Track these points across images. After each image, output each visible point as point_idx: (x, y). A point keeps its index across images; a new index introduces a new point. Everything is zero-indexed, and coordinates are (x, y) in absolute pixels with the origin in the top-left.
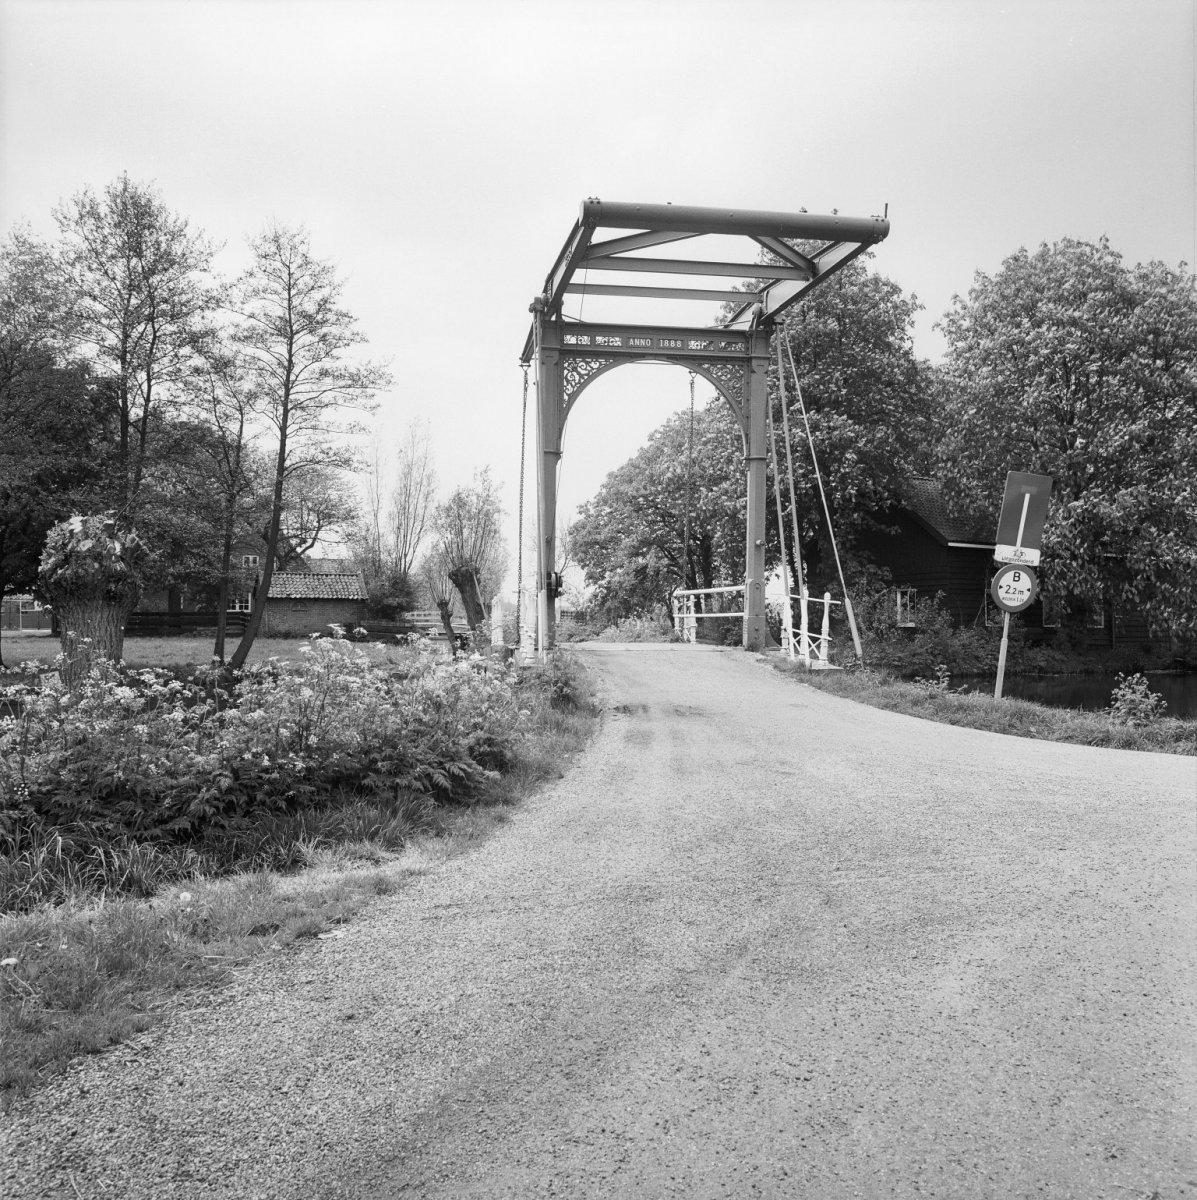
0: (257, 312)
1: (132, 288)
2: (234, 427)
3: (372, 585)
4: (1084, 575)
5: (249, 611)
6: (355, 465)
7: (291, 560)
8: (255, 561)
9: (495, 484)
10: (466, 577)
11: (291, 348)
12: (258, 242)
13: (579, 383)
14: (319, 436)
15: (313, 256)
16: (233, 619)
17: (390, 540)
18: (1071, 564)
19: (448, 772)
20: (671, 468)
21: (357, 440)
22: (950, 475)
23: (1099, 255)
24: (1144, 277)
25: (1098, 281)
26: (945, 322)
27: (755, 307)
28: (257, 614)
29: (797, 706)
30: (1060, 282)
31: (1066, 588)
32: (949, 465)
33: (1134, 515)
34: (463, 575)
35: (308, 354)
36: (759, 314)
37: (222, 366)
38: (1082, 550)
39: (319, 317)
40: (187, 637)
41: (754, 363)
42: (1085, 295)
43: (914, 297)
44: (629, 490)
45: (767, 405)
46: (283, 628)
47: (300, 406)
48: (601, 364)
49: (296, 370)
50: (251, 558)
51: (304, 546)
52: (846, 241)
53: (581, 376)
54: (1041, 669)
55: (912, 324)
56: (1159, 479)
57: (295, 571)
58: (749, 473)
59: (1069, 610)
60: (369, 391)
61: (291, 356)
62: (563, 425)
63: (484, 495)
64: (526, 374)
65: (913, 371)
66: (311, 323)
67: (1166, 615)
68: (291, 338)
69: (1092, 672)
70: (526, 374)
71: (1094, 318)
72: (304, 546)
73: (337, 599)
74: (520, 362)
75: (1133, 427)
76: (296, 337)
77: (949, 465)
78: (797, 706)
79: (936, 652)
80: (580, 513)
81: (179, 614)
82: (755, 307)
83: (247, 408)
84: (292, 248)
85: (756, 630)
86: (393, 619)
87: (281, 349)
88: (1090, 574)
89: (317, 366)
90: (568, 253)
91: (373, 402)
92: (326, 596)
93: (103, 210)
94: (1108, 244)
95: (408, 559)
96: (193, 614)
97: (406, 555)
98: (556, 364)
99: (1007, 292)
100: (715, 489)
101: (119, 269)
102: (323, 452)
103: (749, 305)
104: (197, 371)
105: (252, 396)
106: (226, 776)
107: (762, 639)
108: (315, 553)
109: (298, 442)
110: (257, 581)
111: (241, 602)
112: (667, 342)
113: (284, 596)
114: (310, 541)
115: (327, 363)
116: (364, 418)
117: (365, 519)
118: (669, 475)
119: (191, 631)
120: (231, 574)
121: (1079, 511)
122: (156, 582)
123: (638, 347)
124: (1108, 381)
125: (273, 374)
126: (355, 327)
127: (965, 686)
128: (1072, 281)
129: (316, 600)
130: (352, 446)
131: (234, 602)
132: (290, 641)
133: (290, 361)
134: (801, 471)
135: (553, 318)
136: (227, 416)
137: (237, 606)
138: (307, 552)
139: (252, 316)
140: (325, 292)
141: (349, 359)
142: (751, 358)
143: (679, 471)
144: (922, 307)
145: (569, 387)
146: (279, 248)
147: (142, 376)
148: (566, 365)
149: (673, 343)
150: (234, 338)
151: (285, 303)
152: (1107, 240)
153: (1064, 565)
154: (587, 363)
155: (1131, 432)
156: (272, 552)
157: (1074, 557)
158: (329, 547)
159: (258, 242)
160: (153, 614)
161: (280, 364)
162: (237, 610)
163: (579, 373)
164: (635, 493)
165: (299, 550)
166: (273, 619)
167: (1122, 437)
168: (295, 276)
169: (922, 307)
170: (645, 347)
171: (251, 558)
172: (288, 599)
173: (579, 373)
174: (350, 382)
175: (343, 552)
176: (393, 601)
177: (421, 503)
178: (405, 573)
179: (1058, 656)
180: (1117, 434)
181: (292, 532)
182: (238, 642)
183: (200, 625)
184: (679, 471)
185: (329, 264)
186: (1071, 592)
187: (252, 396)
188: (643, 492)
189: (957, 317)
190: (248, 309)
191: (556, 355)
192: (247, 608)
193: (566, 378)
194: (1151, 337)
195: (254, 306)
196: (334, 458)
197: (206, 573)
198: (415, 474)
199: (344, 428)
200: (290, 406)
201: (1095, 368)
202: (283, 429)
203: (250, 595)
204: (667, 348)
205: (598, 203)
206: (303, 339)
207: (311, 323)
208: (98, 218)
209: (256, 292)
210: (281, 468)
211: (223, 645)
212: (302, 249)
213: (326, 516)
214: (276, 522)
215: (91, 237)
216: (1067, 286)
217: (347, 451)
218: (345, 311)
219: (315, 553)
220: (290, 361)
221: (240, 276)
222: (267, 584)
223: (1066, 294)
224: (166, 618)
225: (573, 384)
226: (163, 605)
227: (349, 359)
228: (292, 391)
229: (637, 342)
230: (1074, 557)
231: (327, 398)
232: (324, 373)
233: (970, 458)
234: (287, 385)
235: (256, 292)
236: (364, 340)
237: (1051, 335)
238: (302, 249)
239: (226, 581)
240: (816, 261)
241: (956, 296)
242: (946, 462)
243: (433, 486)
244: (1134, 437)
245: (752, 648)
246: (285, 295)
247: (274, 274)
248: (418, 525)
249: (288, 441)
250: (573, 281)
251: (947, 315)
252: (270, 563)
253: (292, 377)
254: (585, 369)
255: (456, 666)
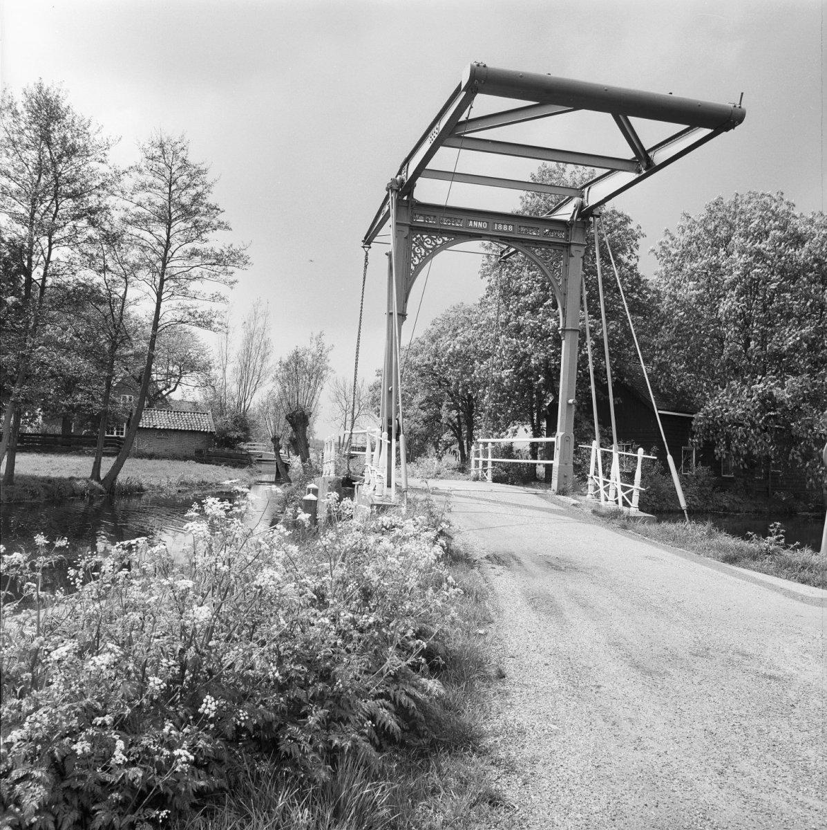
0: (143, 202)
1: (40, 169)
2: (120, 291)
3: (219, 421)
4: (760, 440)
5: (124, 436)
6: (216, 326)
7: (157, 400)
8: (130, 400)
9: (327, 346)
10: (299, 420)
11: (169, 231)
12: (147, 146)
13: (425, 255)
14: (188, 302)
15: (192, 159)
16: (110, 441)
17: (233, 388)
18: (750, 431)
19: (394, 702)
20: (451, 345)
21: (218, 306)
22: (663, 360)
23: (776, 204)
24: (811, 221)
25: (777, 223)
26: (658, 249)
27: (576, 201)
28: (129, 440)
29: (651, 558)
30: (748, 222)
31: (747, 448)
32: (663, 352)
33: (800, 397)
34: (297, 417)
35: (182, 238)
36: (581, 207)
37: (112, 239)
38: (760, 422)
39: (193, 208)
40: (75, 454)
41: (573, 248)
42: (767, 233)
43: (639, 227)
44: (417, 360)
45: (582, 285)
46: (149, 451)
47: (173, 277)
48: (443, 240)
49: (172, 249)
50: (128, 397)
51: (168, 390)
52: (700, 127)
53: (427, 250)
54: (725, 509)
55: (637, 247)
56: (818, 371)
57: (160, 408)
58: (563, 342)
59: (746, 466)
60: (230, 269)
61: (169, 238)
62: (410, 288)
63: (318, 354)
64: (367, 254)
65: (637, 282)
66: (187, 213)
67: (821, 472)
68: (170, 225)
69: (761, 512)
70: (367, 254)
71: (774, 250)
72: (168, 390)
73: (192, 431)
74: (362, 244)
75: (803, 331)
76: (173, 224)
77: (663, 352)
78: (651, 558)
79: (651, 493)
80: (378, 375)
81: (70, 436)
82: (576, 201)
83: (131, 278)
84: (175, 153)
85: (565, 476)
86: (233, 448)
87: (162, 232)
88: (765, 440)
89: (188, 247)
90: (435, 129)
91: (231, 279)
92: (183, 429)
93: (20, 108)
94: (783, 197)
95: (247, 402)
96: (81, 437)
97: (245, 400)
98: (406, 238)
99: (709, 227)
100: (485, 363)
101: (32, 155)
102: (190, 314)
103: (571, 198)
104: (90, 240)
105: (136, 267)
106: (39, 781)
107: (570, 486)
108: (176, 396)
109: (170, 306)
110: (131, 414)
111: (117, 429)
112: (500, 226)
113: (151, 427)
114: (173, 386)
115: (197, 245)
116: (224, 290)
117: (216, 372)
118: (450, 350)
119: (78, 450)
120: (109, 408)
121: (760, 391)
122: (54, 410)
123: (475, 228)
124: (784, 297)
125: (154, 251)
126: (221, 217)
127: (797, 543)
128: (756, 222)
129: (175, 431)
130: (214, 310)
131: (112, 429)
132: (153, 461)
133: (168, 241)
134: (552, 351)
135: (405, 198)
136: (114, 281)
137: (115, 433)
138: (170, 395)
139: (139, 205)
140: (200, 189)
141: (215, 241)
142: (570, 244)
143: (458, 347)
144: (644, 236)
145: (416, 259)
146: (163, 153)
147: (45, 241)
148: (414, 239)
149: (505, 228)
150: (124, 220)
151: (166, 197)
152: (782, 194)
153: (745, 431)
154: (432, 239)
155: (802, 334)
156: (144, 394)
157: (753, 426)
158: (187, 391)
159: (147, 146)
160: (51, 435)
161: (160, 244)
162: (115, 435)
163: (425, 248)
164: (420, 363)
165: (164, 393)
166: (141, 444)
167: (794, 338)
168: (175, 176)
169: (644, 236)
170: (483, 229)
171: (128, 397)
172: (154, 429)
173: (425, 248)
174: (215, 261)
175: (197, 395)
176: (235, 435)
177: (259, 363)
178: (244, 413)
179: (738, 499)
180: (790, 336)
181: (160, 378)
182: (113, 460)
183: (85, 445)
184: (458, 347)
185: (203, 167)
186: (750, 453)
187: (136, 267)
188: (426, 362)
189: (667, 246)
190: (136, 199)
191: (407, 230)
192: (122, 434)
193: (414, 251)
194: (815, 265)
195: (142, 196)
196: (199, 319)
197: (91, 406)
198: (255, 340)
199: (207, 297)
200: (165, 277)
201: (774, 287)
202: (159, 295)
203: (125, 424)
204: (505, 232)
205: (485, 66)
206: (178, 225)
207: (187, 213)
208: (15, 113)
209: (143, 186)
210: (155, 325)
211: (100, 463)
212: (182, 154)
213: (189, 365)
214: (148, 371)
215: (9, 129)
216: (752, 225)
217: (210, 314)
218: (213, 204)
219: (176, 396)
220: (168, 241)
221: (131, 165)
222: (139, 417)
223: (752, 231)
224: (59, 439)
225: (419, 255)
226: (58, 430)
227: (215, 241)
228: (168, 265)
229: (476, 224)
230: (753, 426)
231: (195, 272)
232: (195, 253)
233: (678, 348)
234: (165, 260)
235: (143, 186)
236: (227, 228)
237: (742, 261)
238: (182, 154)
239: (105, 412)
240: (650, 155)
241: (667, 230)
242: (661, 350)
243: (268, 350)
244: (804, 339)
245: (562, 492)
246: (167, 190)
247: (159, 173)
248: (256, 377)
249: (162, 305)
250: (428, 167)
251: (661, 243)
252: (141, 403)
253: (169, 254)
254: (431, 244)
255: (381, 538)
